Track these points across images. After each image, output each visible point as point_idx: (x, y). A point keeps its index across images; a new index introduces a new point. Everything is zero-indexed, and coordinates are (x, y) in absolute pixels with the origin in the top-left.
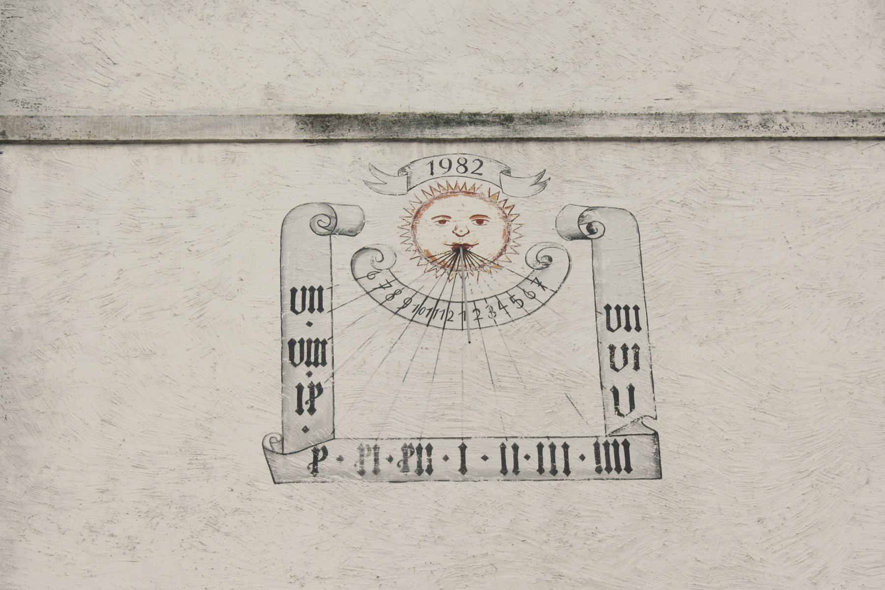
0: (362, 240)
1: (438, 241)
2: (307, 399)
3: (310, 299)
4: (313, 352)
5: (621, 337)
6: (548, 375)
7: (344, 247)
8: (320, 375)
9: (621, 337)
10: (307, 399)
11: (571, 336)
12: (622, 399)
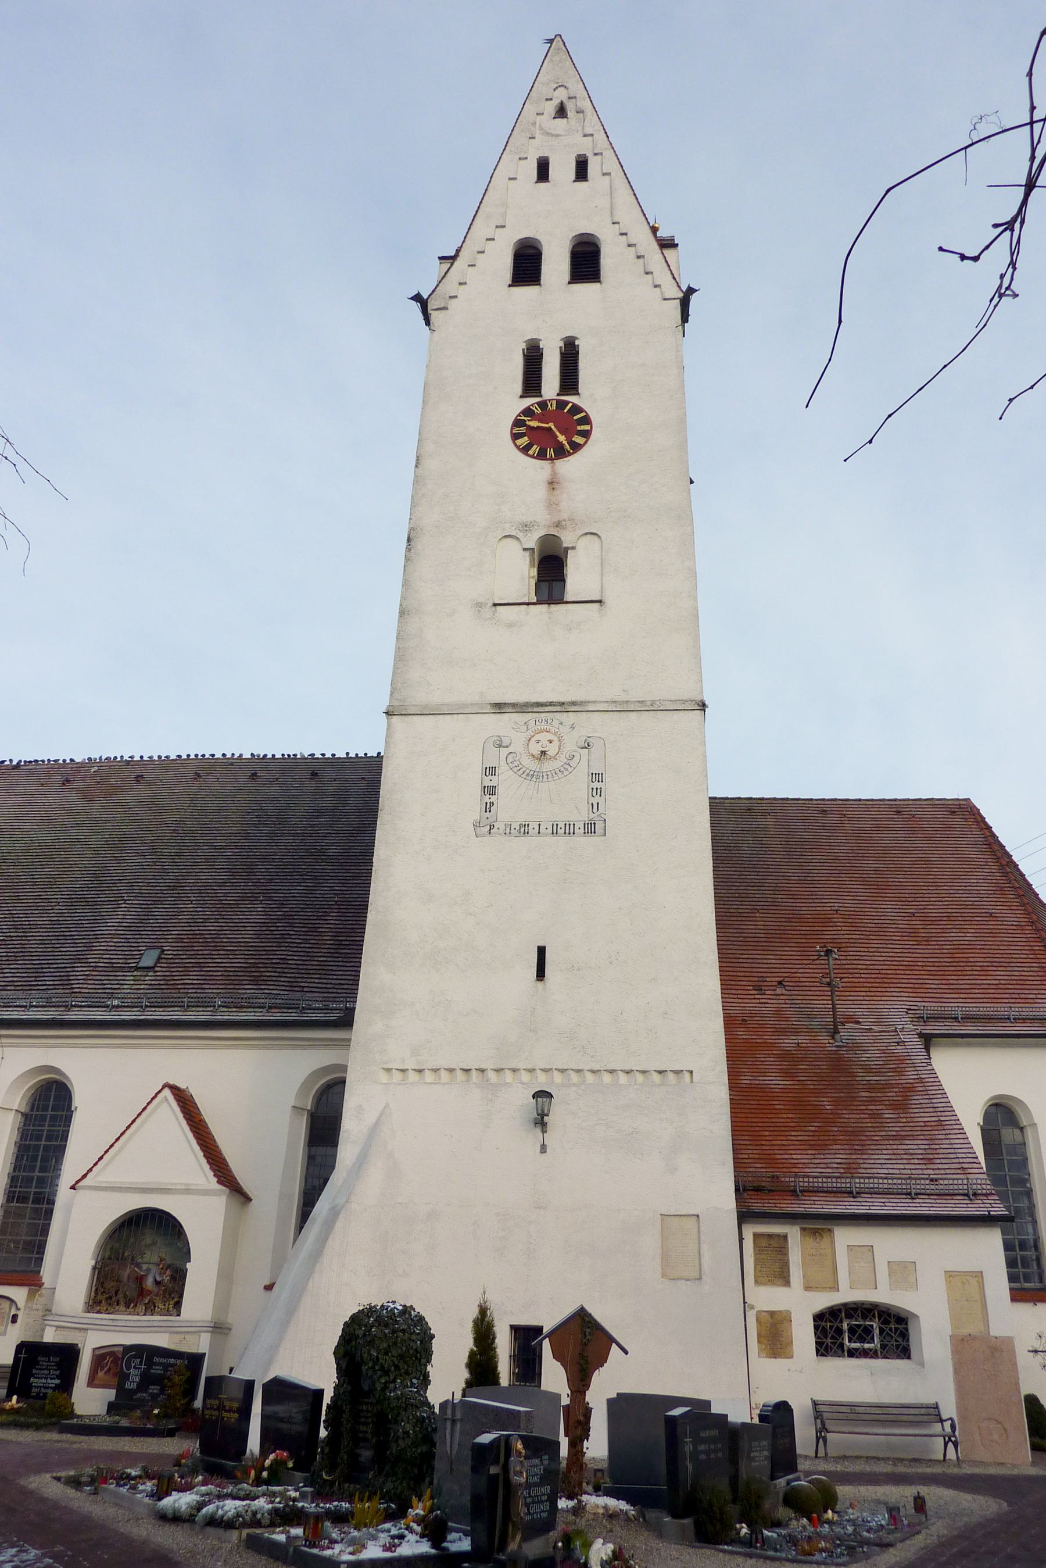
0: (510, 749)
1: (536, 749)
2: (488, 807)
3: (491, 771)
4: (490, 790)
5: (596, 785)
6: (570, 800)
7: (504, 752)
8: (493, 798)
9: (596, 785)
10: (488, 807)
11: (579, 784)
12: (594, 807)
